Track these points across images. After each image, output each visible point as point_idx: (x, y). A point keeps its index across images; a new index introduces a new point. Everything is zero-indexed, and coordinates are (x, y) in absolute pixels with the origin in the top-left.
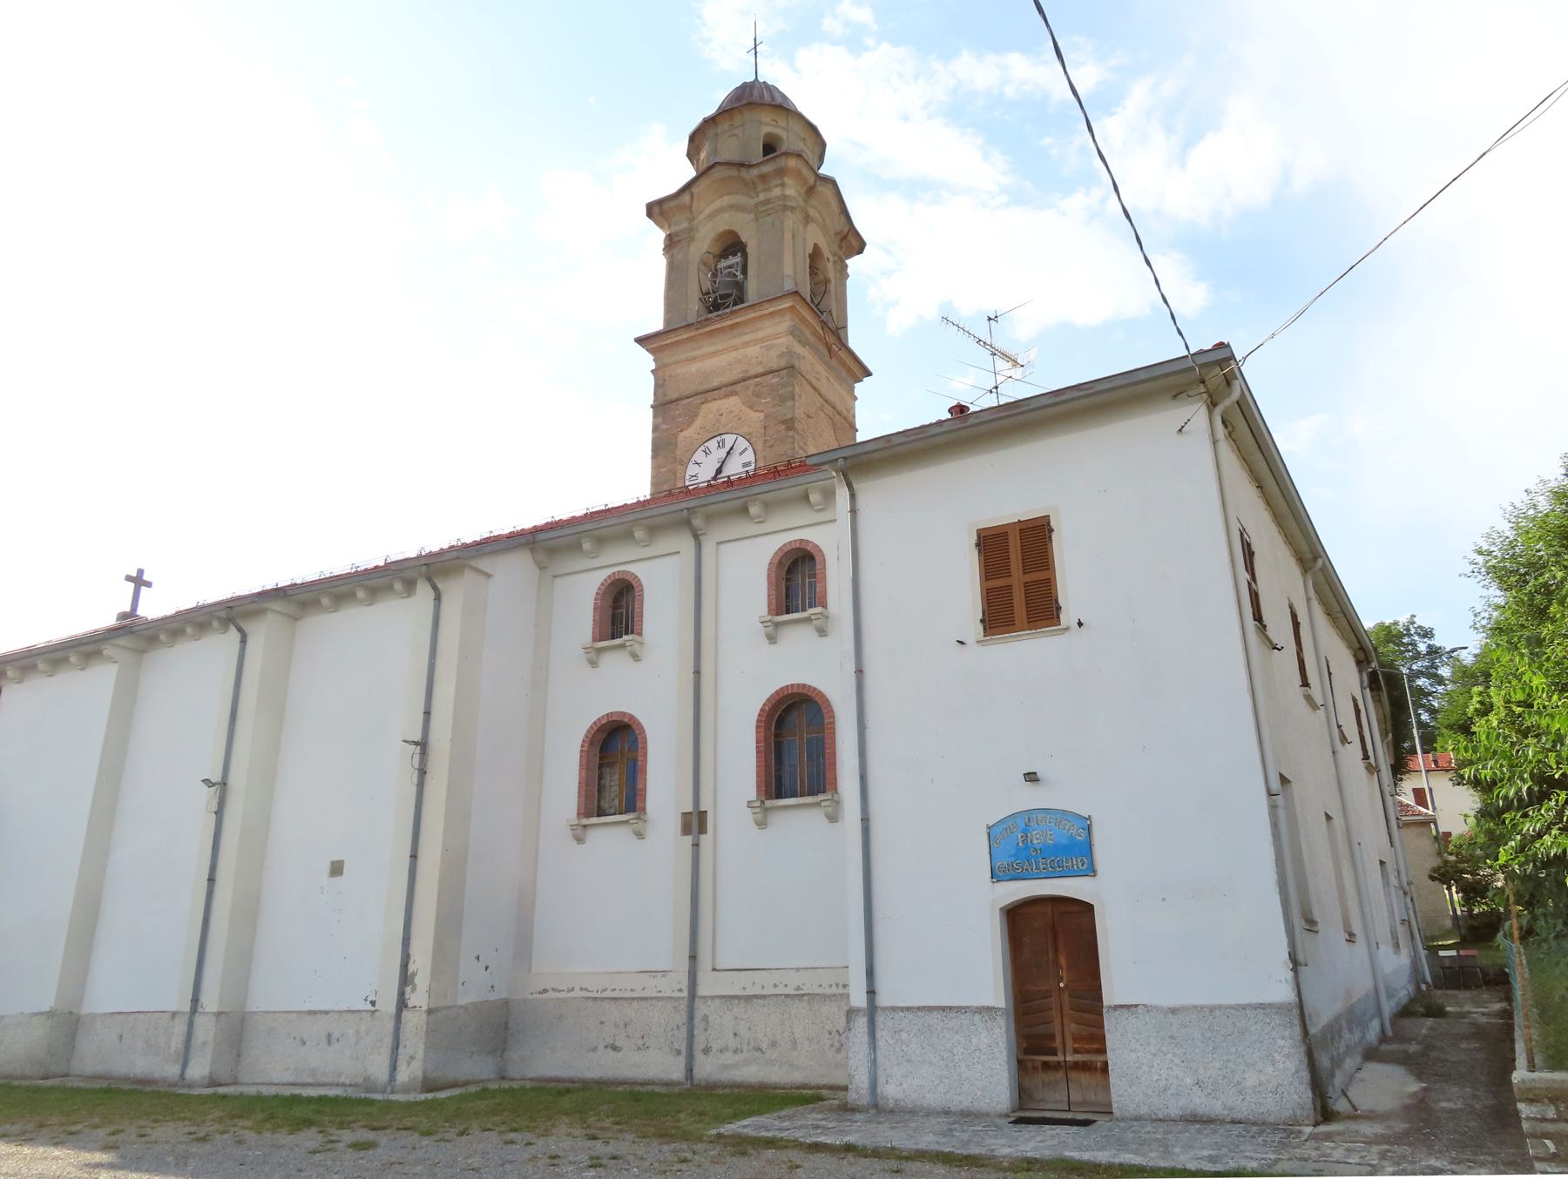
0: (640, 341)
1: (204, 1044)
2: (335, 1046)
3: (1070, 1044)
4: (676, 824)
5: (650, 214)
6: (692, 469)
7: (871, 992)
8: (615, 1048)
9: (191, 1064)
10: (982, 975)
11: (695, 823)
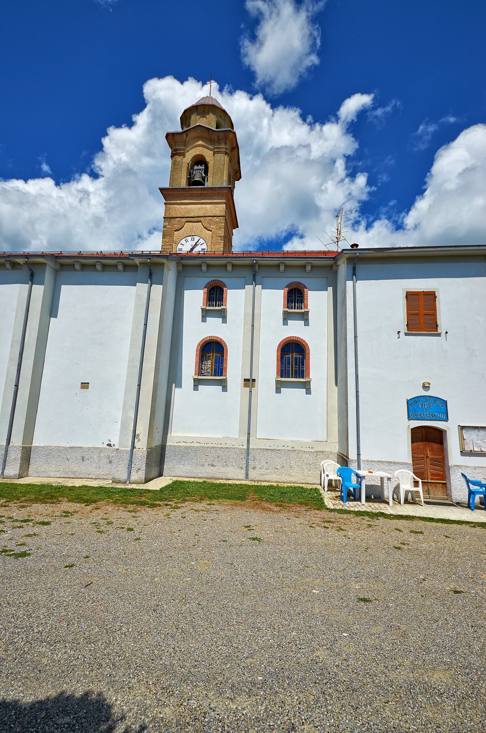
0: (161, 190)
1: (15, 459)
2: (87, 462)
3: (429, 477)
4: (241, 382)
5: (167, 137)
6: (180, 246)
7: (359, 455)
8: (213, 465)
9: (7, 468)
10: (403, 450)
11: (249, 382)
